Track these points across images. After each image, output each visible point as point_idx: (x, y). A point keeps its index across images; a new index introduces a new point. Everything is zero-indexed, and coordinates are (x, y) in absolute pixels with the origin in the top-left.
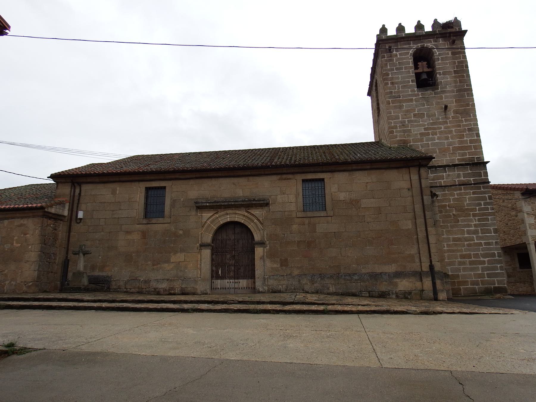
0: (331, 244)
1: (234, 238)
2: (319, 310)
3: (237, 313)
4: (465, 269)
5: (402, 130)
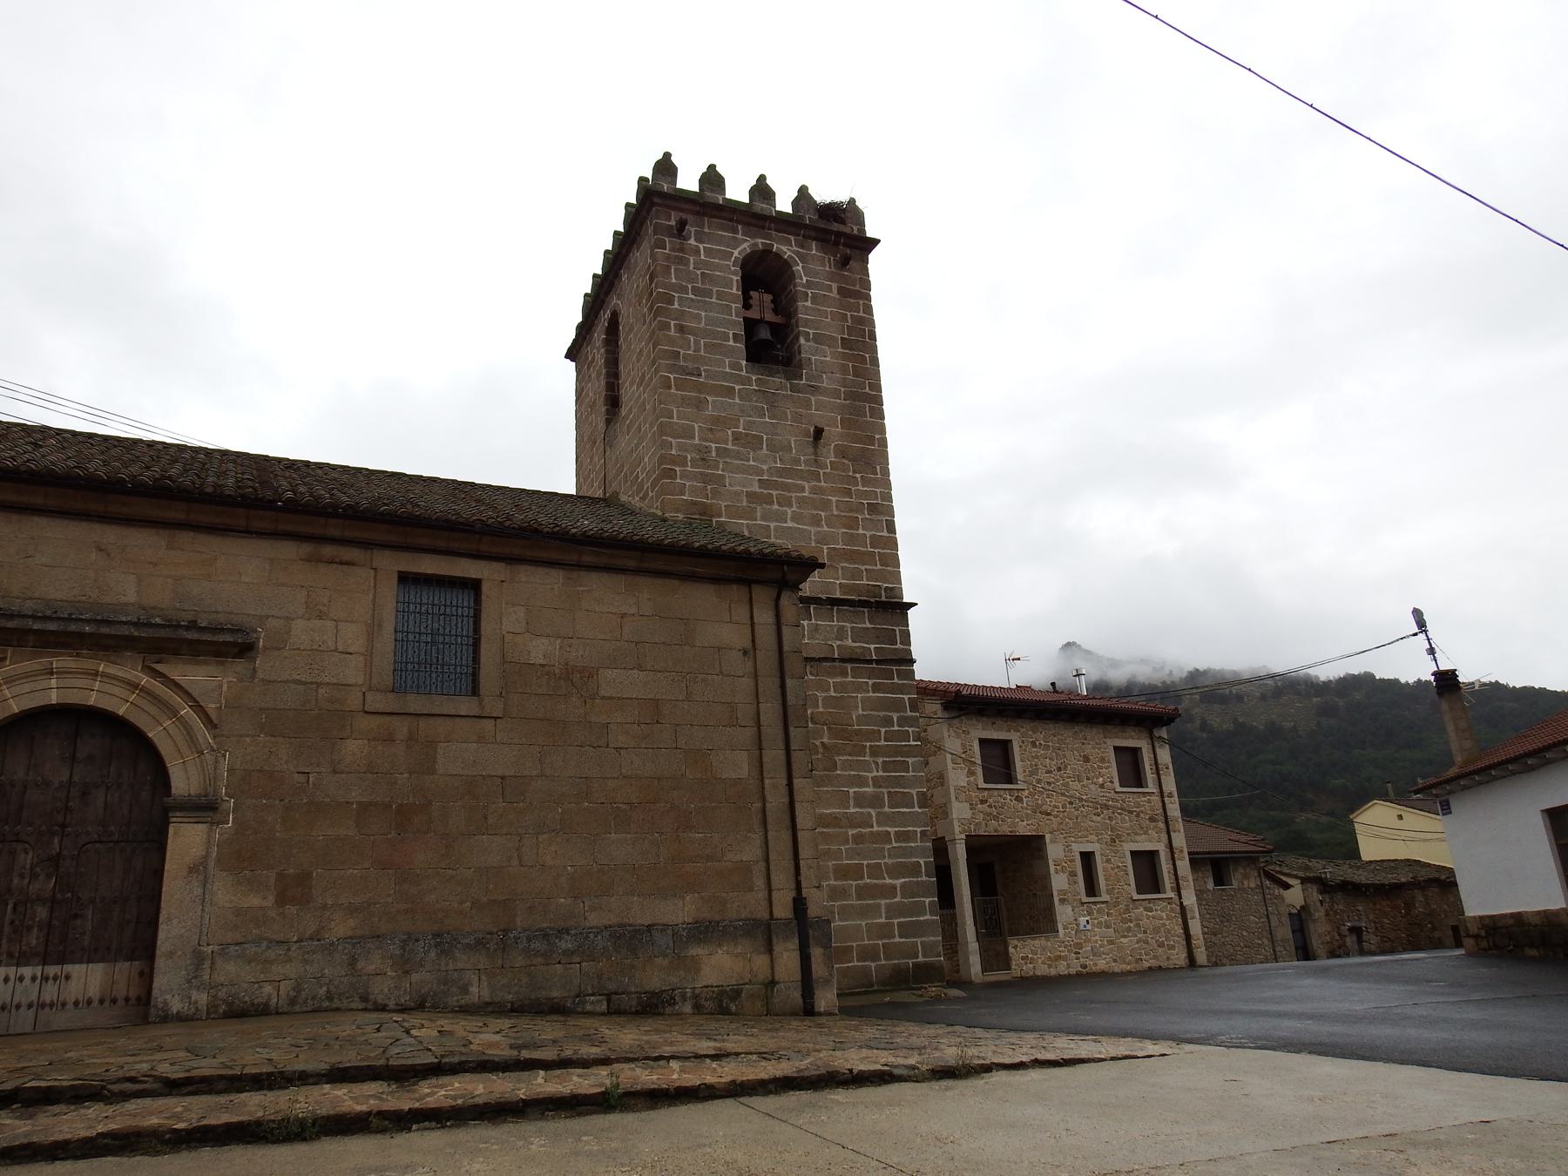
0: (486, 818)
1: (65, 778)
2: (586, 1095)
3: (189, 1148)
4: (845, 912)
5: (701, 473)
